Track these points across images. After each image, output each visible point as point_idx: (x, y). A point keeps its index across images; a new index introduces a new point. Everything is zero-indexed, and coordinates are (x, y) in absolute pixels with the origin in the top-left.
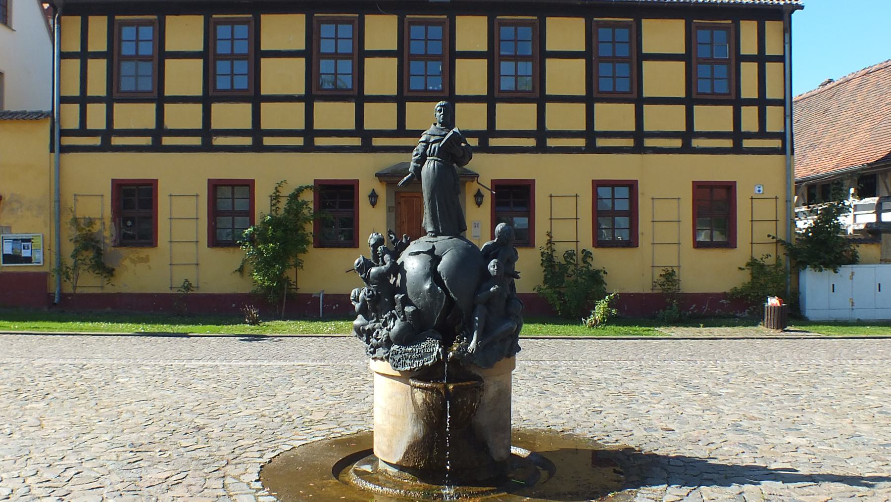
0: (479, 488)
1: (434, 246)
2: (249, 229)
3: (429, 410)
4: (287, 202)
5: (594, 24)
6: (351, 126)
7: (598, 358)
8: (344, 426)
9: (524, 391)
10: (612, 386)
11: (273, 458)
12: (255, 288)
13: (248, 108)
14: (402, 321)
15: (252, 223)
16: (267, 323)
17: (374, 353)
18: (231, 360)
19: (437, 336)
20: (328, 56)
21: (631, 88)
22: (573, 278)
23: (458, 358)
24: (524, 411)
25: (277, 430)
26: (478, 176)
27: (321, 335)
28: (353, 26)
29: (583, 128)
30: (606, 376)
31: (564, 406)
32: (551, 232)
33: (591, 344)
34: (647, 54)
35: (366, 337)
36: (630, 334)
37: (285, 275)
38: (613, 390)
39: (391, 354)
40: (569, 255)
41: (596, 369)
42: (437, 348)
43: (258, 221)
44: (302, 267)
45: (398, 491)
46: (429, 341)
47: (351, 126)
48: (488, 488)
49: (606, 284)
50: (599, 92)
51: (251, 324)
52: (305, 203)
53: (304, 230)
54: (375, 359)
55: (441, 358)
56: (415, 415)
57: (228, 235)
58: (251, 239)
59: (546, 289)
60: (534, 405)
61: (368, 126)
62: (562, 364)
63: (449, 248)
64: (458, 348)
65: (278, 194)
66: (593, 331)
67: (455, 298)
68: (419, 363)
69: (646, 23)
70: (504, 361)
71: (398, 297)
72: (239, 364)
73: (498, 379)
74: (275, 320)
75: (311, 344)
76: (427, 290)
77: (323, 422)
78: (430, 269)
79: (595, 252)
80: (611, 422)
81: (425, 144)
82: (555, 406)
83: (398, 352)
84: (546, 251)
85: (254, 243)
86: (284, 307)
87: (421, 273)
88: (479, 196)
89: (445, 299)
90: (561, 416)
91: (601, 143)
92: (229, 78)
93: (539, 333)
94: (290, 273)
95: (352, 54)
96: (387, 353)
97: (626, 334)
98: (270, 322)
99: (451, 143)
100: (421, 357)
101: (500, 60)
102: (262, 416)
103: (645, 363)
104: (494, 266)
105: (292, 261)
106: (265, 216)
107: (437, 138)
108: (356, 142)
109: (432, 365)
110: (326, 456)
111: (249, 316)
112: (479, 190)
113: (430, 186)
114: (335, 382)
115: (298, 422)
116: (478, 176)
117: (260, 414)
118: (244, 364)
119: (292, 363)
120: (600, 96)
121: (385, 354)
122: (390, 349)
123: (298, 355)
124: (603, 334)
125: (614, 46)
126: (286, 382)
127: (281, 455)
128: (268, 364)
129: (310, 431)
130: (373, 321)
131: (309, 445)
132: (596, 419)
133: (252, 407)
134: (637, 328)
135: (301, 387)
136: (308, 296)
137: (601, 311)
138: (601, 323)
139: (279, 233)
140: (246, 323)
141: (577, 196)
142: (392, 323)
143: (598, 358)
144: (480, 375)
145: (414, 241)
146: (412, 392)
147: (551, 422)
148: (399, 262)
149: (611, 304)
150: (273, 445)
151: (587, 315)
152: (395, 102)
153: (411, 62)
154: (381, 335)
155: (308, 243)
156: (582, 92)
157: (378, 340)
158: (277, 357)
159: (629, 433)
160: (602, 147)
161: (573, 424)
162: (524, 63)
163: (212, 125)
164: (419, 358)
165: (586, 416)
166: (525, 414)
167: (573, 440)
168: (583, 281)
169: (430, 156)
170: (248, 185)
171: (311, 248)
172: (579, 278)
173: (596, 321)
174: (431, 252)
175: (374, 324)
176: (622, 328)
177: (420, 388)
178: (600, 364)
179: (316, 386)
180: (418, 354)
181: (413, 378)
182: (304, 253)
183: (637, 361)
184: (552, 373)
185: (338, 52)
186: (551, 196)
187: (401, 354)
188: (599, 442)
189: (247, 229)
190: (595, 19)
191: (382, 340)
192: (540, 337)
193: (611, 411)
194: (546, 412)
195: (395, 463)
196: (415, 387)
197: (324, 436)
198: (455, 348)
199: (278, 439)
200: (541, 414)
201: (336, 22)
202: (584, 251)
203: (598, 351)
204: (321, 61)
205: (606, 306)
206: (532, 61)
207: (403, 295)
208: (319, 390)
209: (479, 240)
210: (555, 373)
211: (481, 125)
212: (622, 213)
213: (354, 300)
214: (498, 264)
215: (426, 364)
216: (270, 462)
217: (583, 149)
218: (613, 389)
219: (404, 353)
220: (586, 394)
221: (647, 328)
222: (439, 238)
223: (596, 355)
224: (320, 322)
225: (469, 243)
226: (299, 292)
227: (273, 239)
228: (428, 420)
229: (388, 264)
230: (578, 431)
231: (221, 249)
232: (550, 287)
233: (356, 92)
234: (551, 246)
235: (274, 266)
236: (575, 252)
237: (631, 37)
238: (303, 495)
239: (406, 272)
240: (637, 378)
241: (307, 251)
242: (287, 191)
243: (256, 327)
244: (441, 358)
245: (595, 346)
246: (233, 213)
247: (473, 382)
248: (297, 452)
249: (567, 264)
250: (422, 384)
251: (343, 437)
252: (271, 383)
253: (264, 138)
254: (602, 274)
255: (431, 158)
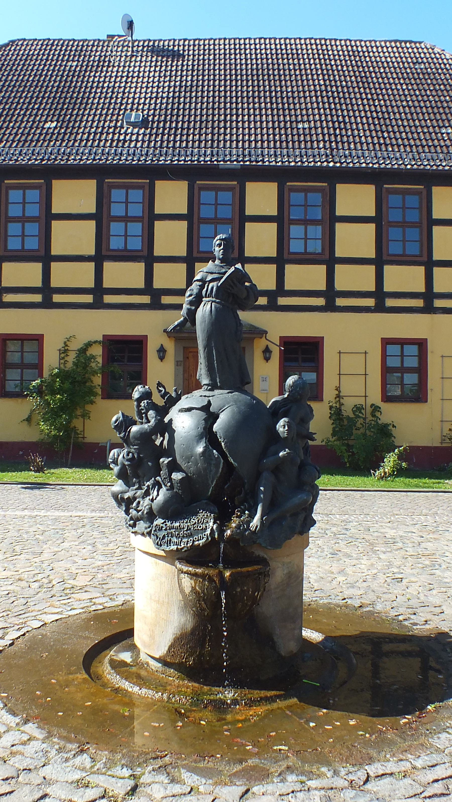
0: (262, 692)
1: (209, 402)
2: (36, 381)
3: (199, 601)
4: (76, 355)
5: (384, 190)
6: (141, 284)
7: (390, 512)
8: (109, 595)
9: (313, 551)
10: (410, 546)
11: (17, 638)
12: (42, 437)
13: (38, 267)
14: (167, 490)
15: (41, 375)
16: (52, 471)
17: (134, 526)
18: (8, 509)
19: (212, 508)
20: (118, 219)
21: (421, 251)
22: (362, 430)
23: (237, 537)
24: (315, 577)
25: (32, 599)
26: (266, 332)
27: (105, 484)
28: (143, 192)
29: (372, 288)
30: (401, 533)
31: (360, 570)
32: (339, 387)
33: (381, 496)
34: (437, 220)
35: (125, 506)
36: (421, 486)
37: (72, 425)
38: (411, 551)
39: (154, 529)
40: (358, 409)
41: (389, 525)
42: (211, 524)
43: (46, 374)
44: (89, 417)
45: (160, 694)
46: (202, 515)
47: (141, 284)
48: (273, 693)
49: (395, 438)
50: (389, 255)
51: (36, 471)
52: (93, 357)
53: (92, 382)
54: (135, 533)
55: (216, 537)
56: (183, 602)
57: (16, 386)
58: (39, 391)
59: (334, 441)
60: (326, 570)
61: (157, 284)
62: (353, 518)
63: (228, 403)
64: (238, 525)
65: (66, 348)
66: (382, 483)
67: (235, 464)
68: (187, 542)
69: (436, 190)
70: (296, 539)
71: (164, 461)
72: (15, 514)
73: (287, 560)
74: (61, 467)
75: (93, 493)
76: (199, 454)
77: (86, 589)
78: (205, 429)
79: (385, 407)
80: (415, 593)
81: (200, 283)
82: (349, 570)
83: (162, 527)
84: (334, 405)
85: (42, 394)
86: (70, 455)
87: (194, 433)
88: (267, 353)
89: (222, 464)
90: (357, 584)
91: (390, 303)
92: (20, 238)
93: (327, 484)
94: (77, 423)
95: (143, 217)
96: (149, 527)
97: (417, 486)
98: (56, 470)
99: (233, 282)
100: (191, 535)
101: (290, 224)
102: (20, 580)
103: (440, 518)
104: (284, 426)
105: (79, 412)
106: (54, 369)
107: (215, 276)
108: (146, 299)
109: (205, 545)
110: (81, 637)
111: (34, 463)
112: (267, 346)
113: (204, 330)
114: (111, 537)
115: (58, 588)
116: (266, 332)
117: (17, 577)
118: (19, 513)
119: (70, 514)
120: (389, 258)
121: (146, 528)
122: (152, 524)
123: (78, 505)
124: (392, 486)
125: (404, 212)
126: (58, 536)
127: (27, 634)
128: (45, 514)
129: (69, 601)
130: (135, 488)
131: (63, 620)
132: (397, 589)
133: (11, 567)
134: (427, 480)
135: (73, 543)
136: (95, 445)
137: (391, 464)
138: (390, 475)
139: (67, 385)
140: (31, 470)
141: (366, 353)
142: (155, 493)
143: (390, 512)
144: (265, 556)
145: (186, 396)
146: (178, 577)
147: (348, 593)
148: (166, 420)
149: (401, 457)
150: (21, 621)
151: (377, 467)
152: (184, 263)
153: (201, 225)
154: (142, 506)
155: (95, 395)
156: (372, 255)
157: (138, 511)
158: (56, 506)
159: (438, 610)
160: (392, 307)
161: (371, 597)
162: (314, 227)
163: (2, 283)
164: (189, 536)
165: (385, 585)
166: (316, 581)
167: (375, 620)
168: (372, 434)
169: (206, 297)
170: (37, 340)
171: (98, 399)
172: (367, 431)
173: (385, 473)
174: (206, 408)
175: (135, 492)
176: (411, 480)
177: (188, 574)
178: (392, 518)
179: (88, 542)
180: (186, 531)
181: (181, 560)
182: (92, 404)
183: (431, 516)
184: (343, 529)
185: (129, 215)
186: (340, 353)
187: (166, 530)
188: (406, 623)
189: (35, 381)
190: (385, 186)
191: (143, 513)
192: (328, 488)
193: (413, 579)
194: (341, 578)
195: (158, 657)
196: (182, 572)
197: (82, 608)
198: (234, 525)
199: (29, 612)
200: (334, 582)
201: (127, 187)
202: (372, 405)
203: (390, 505)
204: (111, 223)
205: (396, 459)
206: (321, 224)
207: (170, 459)
208: (90, 547)
209: (267, 393)
210: (347, 529)
211: (271, 285)
212: (410, 370)
213: (113, 462)
214: (289, 424)
215: (196, 543)
216: (11, 645)
217: (373, 308)
218: (411, 549)
219: (170, 529)
220: (382, 556)
221: (437, 481)
222: (217, 392)
223: (387, 509)
224: (105, 470)
225: (254, 398)
226: (87, 440)
227: (61, 391)
228: (197, 611)
229: (153, 422)
230: (379, 607)
231: (10, 399)
232: (338, 440)
233: (145, 253)
234: (339, 400)
235: (61, 416)
236: (364, 407)
237: (421, 203)
238: (39, 697)
239: (174, 431)
240: (435, 536)
241: (94, 402)
242: (75, 346)
243: (41, 474)
244: (216, 537)
245: (386, 499)
246: (22, 366)
247: (256, 567)
248: (46, 631)
249: (356, 418)
250: (190, 569)
251: (106, 611)
252: (41, 538)
253: (54, 295)
254: (391, 427)
255: (208, 299)
